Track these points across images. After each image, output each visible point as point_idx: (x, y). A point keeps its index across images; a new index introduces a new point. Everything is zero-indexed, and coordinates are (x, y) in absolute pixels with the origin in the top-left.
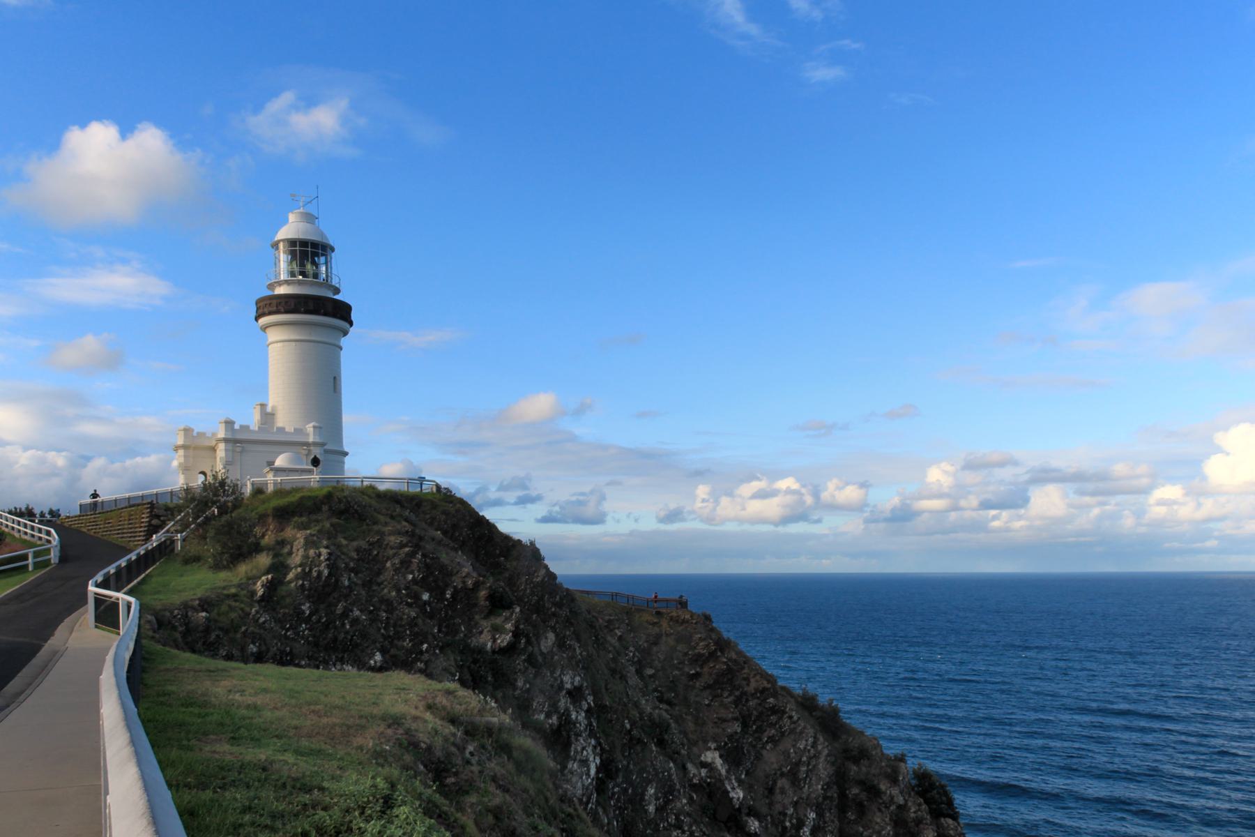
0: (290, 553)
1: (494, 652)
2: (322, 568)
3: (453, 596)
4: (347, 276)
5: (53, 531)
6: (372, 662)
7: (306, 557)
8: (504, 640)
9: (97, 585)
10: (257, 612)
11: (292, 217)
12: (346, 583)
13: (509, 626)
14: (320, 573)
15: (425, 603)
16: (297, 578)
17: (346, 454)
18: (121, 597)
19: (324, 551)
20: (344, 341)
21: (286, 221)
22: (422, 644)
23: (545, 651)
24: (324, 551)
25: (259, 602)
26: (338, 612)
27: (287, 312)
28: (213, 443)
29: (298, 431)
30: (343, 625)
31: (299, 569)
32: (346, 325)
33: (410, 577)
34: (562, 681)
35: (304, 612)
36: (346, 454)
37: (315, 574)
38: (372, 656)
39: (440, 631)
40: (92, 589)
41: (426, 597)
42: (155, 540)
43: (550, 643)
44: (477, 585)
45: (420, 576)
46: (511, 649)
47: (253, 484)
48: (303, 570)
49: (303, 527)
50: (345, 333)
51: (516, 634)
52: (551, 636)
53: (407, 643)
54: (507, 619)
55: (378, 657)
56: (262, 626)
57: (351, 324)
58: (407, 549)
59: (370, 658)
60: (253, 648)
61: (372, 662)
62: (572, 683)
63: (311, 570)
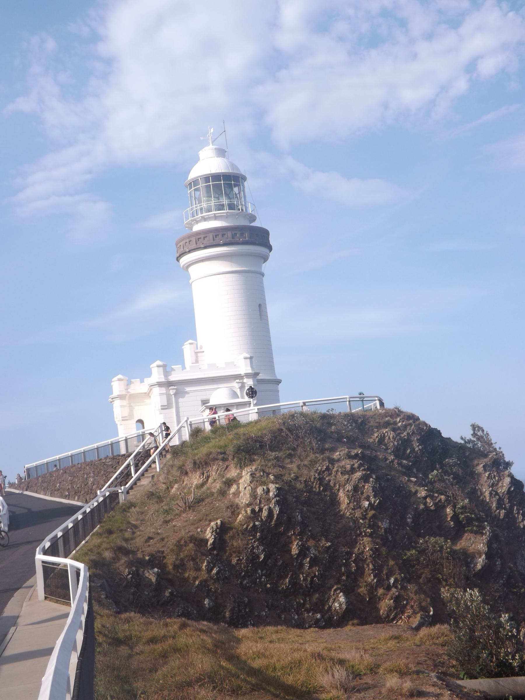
4: (261, 206)
7: (254, 495)
9: (46, 552)
17: (279, 382)
20: (266, 267)
24: (272, 487)
31: (249, 510)
36: (279, 382)
37: (265, 513)
40: (40, 557)
48: (253, 511)
50: (265, 259)
57: (270, 248)
61: (337, 605)
63: (261, 510)
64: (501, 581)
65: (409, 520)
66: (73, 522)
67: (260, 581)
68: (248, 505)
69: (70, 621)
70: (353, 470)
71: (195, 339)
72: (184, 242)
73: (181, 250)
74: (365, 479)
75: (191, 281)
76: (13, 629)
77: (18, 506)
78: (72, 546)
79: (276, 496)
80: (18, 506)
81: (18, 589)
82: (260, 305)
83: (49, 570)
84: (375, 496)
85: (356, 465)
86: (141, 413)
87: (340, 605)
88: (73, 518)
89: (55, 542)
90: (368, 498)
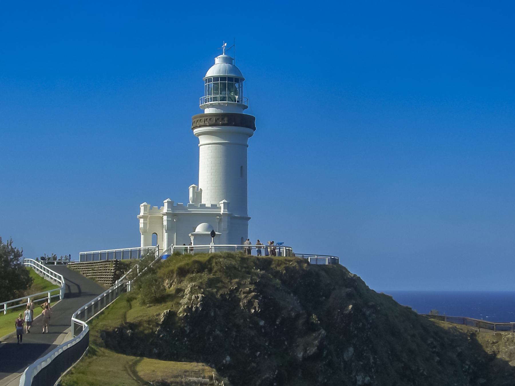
1: (305, 359)
2: (198, 306)
4: (252, 100)
5: (62, 276)
6: (224, 361)
7: (190, 299)
8: (312, 350)
9: (77, 317)
11: (217, 60)
12: (212, 314)
13: (316, 342)
14: (197, 308)
15: (261, 327)
16: (185, 310)
17: (250, 218)
18: (84, 324)
19: (200, 295)
20: (249, 141)
21: (213, 63)
22: (257, 351)
24: (200, 295)
25: (161, 325)
26: (206, 331)
27: (210, 125)
28: (162, 215)
29: (214, 206)
31: (186, 307)
32: (251, 130)
33: (253, 311)
34: (356, 380)
35: (185, 331)
37: (194, 309)
38: (224, 358)
39: (270, 344)
41: (262, 323)
42: (118, 283)
44: (298, 316)
45: (316, 292)
46: (317, 357)
47: (174, 250)
48: (188, 307)
49: (192, 280)
50: (250, 135)
51: (321, 348)
52: (351, 349)
53: (247, 351)
54: (316, 338)
55: (228, 358)
56: (161, 339)
58: (253, 294)
60: (156, 351)
61: (224, 361)
63: (192, 307)
64: (324, 363)
65: (277, 323)
67: (185, 344)
68: (186, 304)
70: (250, 292)
72: (197, 119)
73: (195, 125)
74: (255, 297)
75: (199, 145)
76: (169, 381)
77: (75, 284)
79: (201, 301)
80: (75, 284)
81: (61, 333)
82: (242, 167)
83: (76, 325)
84: (259, 308)
86: (154, 235)
87: (226, 362)
88: (96, 299)
89: (83, 312)
90: (255, 308)
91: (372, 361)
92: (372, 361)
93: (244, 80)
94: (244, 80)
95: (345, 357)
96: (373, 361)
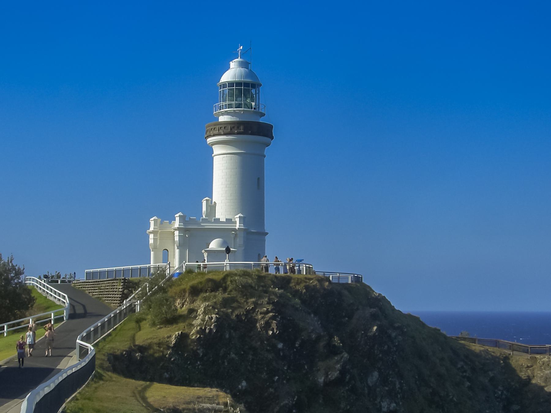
0: (196, 317)
1: (326, 384)
2: (212, 327)
3: (300, 345)
4: (270, 107)
6: (240, 387)
7: (203, 320)
8: (334, 375)
9: (82, 340)
10: (170, 354)
11: (233, 64)
12: (227, 336)
14: (211, 330)
15: (280, 350)
16: (198, 332)
17: (267, 234)
18: (90, 346)
21: (228, 68)
22: (275, 376)
23: (371, 385)
24: (214, 316)
25: (172, 348)
27: (225, 134)
28: (173, 230)
29: (229, 221)
30: (224, 362)
31: (198, 328)
32: (269, 139)
33: (271, 333)
34: (381, 406)
36: (267, 234)
37: (207, 331)
41: (280, 346)
42: (126, 303)
43: (375, 379)
44: (319, 338)
45: (338, 313)
46: (339, 382)
48: (201, 328)
49: (205, 299)
50: (268, 145)
51: (343, 372)
52: (376, 374)
53: (264, 376)
54: (338, 362)
55: (244, 383)
56: (173, 363)
57: (272, 138)
58: (271, 314)
59: (239, 384)
60: (166, 375)
62: (388, 408)
64: (347, 388)
65: (297, 345)
66: (101, 322)
67: (198, 368)
68: (199, 325)
69: (208, 389)
70: (267, 312)
71: (211, 197)
73: (208, 134)
74: (273, 318)
75: (213, 155)
78: (122, 318)
79: (215, 322)
81: (65, 356)
82: (258, 179)
83: (82, 348)
84: (277, 329)
85: (270, 310)
87: (242, 387)
89: (89, 334)
90: (273, 330)
91: (398, 386)
92: (398, 386)
93: (261, 85)
94: (261, 85)
95: (369, 382)
96: (399, 386)
